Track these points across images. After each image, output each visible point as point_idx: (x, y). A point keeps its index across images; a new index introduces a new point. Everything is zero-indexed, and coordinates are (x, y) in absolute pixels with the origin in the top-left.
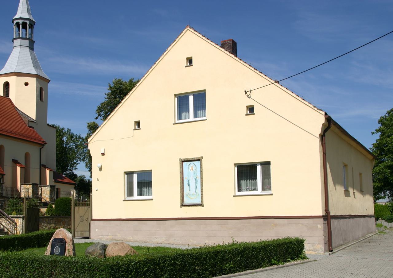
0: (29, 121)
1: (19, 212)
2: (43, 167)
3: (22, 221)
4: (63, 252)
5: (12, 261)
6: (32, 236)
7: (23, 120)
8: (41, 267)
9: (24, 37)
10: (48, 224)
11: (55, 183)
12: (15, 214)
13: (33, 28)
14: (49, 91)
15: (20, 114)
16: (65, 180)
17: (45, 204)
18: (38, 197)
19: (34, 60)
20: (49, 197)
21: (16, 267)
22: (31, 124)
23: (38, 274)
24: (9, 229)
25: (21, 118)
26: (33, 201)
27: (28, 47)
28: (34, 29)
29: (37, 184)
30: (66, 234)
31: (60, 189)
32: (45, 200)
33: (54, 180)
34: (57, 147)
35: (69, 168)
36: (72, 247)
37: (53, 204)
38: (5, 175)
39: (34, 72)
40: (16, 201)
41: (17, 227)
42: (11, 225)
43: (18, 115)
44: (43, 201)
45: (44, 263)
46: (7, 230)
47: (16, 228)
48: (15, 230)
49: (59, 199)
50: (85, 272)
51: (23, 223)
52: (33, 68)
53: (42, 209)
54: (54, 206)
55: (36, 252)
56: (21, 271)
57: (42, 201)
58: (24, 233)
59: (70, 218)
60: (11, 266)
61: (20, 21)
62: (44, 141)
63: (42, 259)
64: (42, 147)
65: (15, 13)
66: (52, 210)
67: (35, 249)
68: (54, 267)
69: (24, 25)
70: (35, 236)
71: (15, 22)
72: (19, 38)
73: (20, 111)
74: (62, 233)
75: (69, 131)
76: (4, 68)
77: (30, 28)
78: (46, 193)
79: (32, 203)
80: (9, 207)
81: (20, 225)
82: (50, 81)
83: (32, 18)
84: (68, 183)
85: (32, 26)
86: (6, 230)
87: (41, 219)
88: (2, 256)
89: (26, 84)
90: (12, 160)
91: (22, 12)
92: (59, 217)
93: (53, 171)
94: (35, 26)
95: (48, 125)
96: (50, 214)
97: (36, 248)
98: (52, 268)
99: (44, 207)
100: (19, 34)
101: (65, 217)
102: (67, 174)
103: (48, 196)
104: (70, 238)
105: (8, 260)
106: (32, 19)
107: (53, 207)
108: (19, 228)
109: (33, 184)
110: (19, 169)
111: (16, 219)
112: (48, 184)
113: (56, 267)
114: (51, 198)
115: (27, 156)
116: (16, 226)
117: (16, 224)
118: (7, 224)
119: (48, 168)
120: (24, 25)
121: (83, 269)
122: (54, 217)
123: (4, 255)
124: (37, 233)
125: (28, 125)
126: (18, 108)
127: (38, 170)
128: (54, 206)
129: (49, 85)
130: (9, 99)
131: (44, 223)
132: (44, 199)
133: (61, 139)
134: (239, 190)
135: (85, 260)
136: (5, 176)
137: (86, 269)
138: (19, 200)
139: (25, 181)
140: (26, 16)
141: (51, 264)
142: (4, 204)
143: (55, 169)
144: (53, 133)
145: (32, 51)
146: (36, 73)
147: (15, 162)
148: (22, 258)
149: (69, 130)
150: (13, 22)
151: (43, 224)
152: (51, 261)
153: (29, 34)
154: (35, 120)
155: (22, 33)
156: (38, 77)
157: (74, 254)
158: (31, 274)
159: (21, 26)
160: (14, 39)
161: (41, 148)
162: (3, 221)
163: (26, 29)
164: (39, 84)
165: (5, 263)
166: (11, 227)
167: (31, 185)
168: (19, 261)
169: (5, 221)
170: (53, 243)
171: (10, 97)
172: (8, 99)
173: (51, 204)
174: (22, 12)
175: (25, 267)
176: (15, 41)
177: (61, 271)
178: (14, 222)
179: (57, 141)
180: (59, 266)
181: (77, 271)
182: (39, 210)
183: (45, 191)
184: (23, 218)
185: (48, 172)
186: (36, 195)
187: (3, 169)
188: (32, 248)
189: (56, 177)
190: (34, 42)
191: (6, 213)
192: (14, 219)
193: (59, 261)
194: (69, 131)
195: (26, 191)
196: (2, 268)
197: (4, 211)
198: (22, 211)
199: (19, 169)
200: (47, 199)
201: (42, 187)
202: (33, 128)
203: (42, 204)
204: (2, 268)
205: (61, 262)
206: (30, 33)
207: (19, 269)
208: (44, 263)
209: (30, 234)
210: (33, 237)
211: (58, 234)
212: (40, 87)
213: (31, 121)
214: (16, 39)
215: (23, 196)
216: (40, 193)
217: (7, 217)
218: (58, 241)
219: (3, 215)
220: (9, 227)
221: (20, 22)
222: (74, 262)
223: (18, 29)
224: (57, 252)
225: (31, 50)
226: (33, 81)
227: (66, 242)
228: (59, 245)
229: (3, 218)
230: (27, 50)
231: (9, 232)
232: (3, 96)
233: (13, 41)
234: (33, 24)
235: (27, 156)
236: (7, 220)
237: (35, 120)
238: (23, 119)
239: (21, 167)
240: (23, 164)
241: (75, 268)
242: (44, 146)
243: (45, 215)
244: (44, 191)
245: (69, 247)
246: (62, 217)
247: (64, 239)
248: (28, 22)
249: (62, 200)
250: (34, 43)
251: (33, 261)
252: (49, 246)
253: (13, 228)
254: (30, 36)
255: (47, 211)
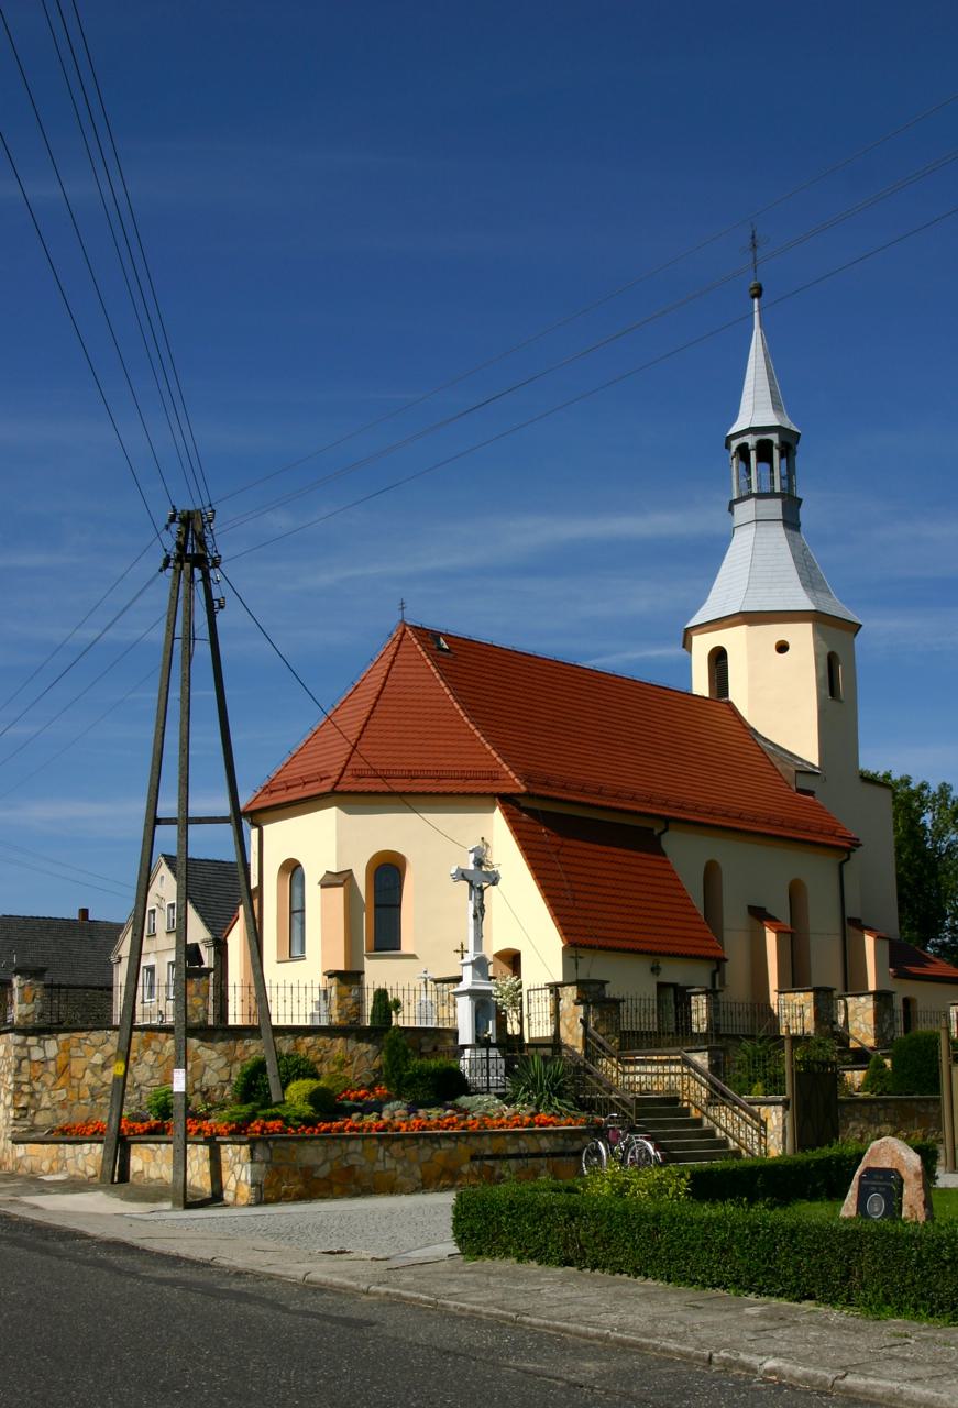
0: (797, 772)
1: (774, 1084)
2: (853, 926)
3: (780, 1114)
4: (893, 1210)
5: (737, 1231)
6: (808, 1163)
7: (777, 770)
8: (817, 1251)
9: (767, 489)
10: (870, 1122)
11: (897, 980)
12: (761, 1090)
13: (795, 454)
14: (860, 659)
15: (766, 750)
16: (932, 970)
17: (861, 1057)
18: (835, 1034)
19: (802, 561)
20: (872, 1033)
21: (748, 1248)
22: (804, 783)
23: (809, 1271)
24: (743, 1141)
25: (772, 764)
26: (820, 1045)
27: (781, 523)
28: (796, 458)
29: (830, 990)
30: (903, 1154)
31: (914, 1000)
32: (860, 1043)
33: (891, 970)
34: (899, 850)
35: (948, 922)
36: (922, 1198)
37: (886, 1056)
38: (726, 960)
39: (804, 603)
40: (761, 1049)
41: (768, 1133)
42: (750, 1128)
43: (762, 755)
44: (853, 1045)
45: (826, 1238)
46: (736, 1144)
47: (765, 1137)
48: (760, 1143)
49: (911, 1033)
50: (944, 1268)
51: (784, 1121)
52: (801, 589)
53: (848, 1074)
54: (888, 1062)
55: (812, 1212)
56: (764, 1262)
57: (851, 1046)
58: (788, 1152)
59: (938, 1102)
60: (734, 1247)
61: (751, 440)
62: (853, 836)
63: (819, 1227)
64: (845, 857)
65: (733, 416)
66: (882, 1077)
67: (818, 1204)
68: (854, 1250)
69: (764, 451)
70: (818, 1163)
71: (735, 444)
72: (750, 496)
73: (766, 740)
74: (892, 1152)
75: (947, 791)
76: (706, 604)
77: (782, 456)
78: (860, 1020)
79: (815, 1053)
80: (739, 1068)
81: (775, 1127)
82: (861, 626)
83: (787, 423)
84: (934, 976)
85: (788, 450)
86: (733, 1144)
87: (847, 1109)
88: (710, 1218)
89: (782, 648)
90: (746, 908)
91: (756, 409)
92: (907, 1100)
93: (890, 939)
94: (799, 448)
95: (869, 779)
96: (879, 1090)
97: (822, 1200)
98: (850, 1254)
99: (854, 1066)
100: (749, 482)
101: (927, 1101)
102: (943, 946)
103: (869, 1030)
104: (916, 1168)
105: (725, 1228)
106: (787, 427)
107: (885, 1066)
108: (772, 1137)
109: (817, 991)
110: (771, 938)
111: (763, 1108)
112: (872, 987)
113: (859, 1251)
114: (880, 1034)
115: (796, 892)
116: (765, 1130)
117: (763, 1124)
118: (735, 1126)
119: (871, 930)
120: (764, 451)
121: (939, 1259)
122: (891, 1100)
123: (714, 1214)
124: (827, 1151)
125: (794, 788)
126: (760, 732)
127: (837, 940)
128: (888, 1062)
129: (858, 640)
130: (730, 704)
131: (858, 1119)
132: (855, 1039)
133: (914, 822)
134: (846, 991)
135: (944, 1233)
136: (726, 964)
137: (947, 1257)
138: (771, 1046)
139: (794, 979)
140: (769, 418)
141: (846, 1242)
142: (724, 1058)
143: (893, 930)
144: (883, 801)
145: (795, 533)
146: (813, 608)
147: (759, 915)
148: (764, 1221)
149: (945, 789)
150: (728, 446)
151: (851, 1125)
152: (847, 1232)
153: (782, 478)
154: (817, 765)
155: (759, 477)
156: (818, 618)
157: (930, 1217)
158: (791, 1271)
159: (753, 455)
160: (733, 502)
161: (841, 860)
162: (723, 1114)
163: (770, 461)
164: (823, 644)
165: (717, 1237)
166: (748, 1134)
167: (811, 994)
168: (755, 1231)
169: (730, 1116)
170: (865, 1182)
171: (733, 696)
172: (725, 706)
173: (877, 1057)
174: (756, 409)
175: (775, 1250)
176: (737, 507)
177: (874, 1262)
178: (756, 1116)
179: (896, 829)
180: (870, 1249)
181: (920, 1263)
182: (836, 1079)
183: (859, 1011)
184: (786, 1104)
185: (869, 942)
186: (828, 1027)
187: (720, 940)
188: (810, 1200)
189: (900, 958)
190: (800, 500)
191: (733, 1089)
192: (756, 1108)
193: (868, 1233)
194: (947, 791)
195: (795, 1011)
196: (711, 1252)
197: (724, 1083)
198: (782, 1082)
199: (771, 938)
200: (865, 1038)
201: (848, 999)
202: (811, 793)
203: (848, 1057)
204: (711, 1252)
205: (873, 1235)
206: (785, 473)
207: (758, 1256)
208: (826, 1238)
209: (801, 1157)
210: (812, 1165)
211: (875, 1154)
212: (828, 651)
213: (805, 771)
214: (741, 500)
215: (783, 1032)
216: (841, 1019)
217: (735, 1103)
218: (876, 1176)
219: (723, 1094)
220: (742, 1135)
221: (750, 444)
222: (910, 1236)
223: (744, 467)
224: (876, 1210)
225: (790, 532)
226: (801, 636)
227: (902, 1180)
228: (880, 1189)
229: (723, 1104)
230: (779, 531)
231: (744, 1151)
232: (707, 695)
233: (731, 510)
234: (792, 442)
235: (796, 892)
236: (734, 1111)
237: (817, 765)
238: (778, 767)
239: (778, 932)
240: (786, 920)
241: (915, 1254)
242: (852, 854)
243: (861, 1095)
244: (854, 1012)
245: (912, 1194)
246: (918, 1101)
247: (896, 1170)
248: (774, 438)
249: (914, 1042)
250: (800, 504)
251: (793, 1232)
252: (850, 1193)
253: (756, 1139)
254: (785, 482)
255: (866, 1078)
